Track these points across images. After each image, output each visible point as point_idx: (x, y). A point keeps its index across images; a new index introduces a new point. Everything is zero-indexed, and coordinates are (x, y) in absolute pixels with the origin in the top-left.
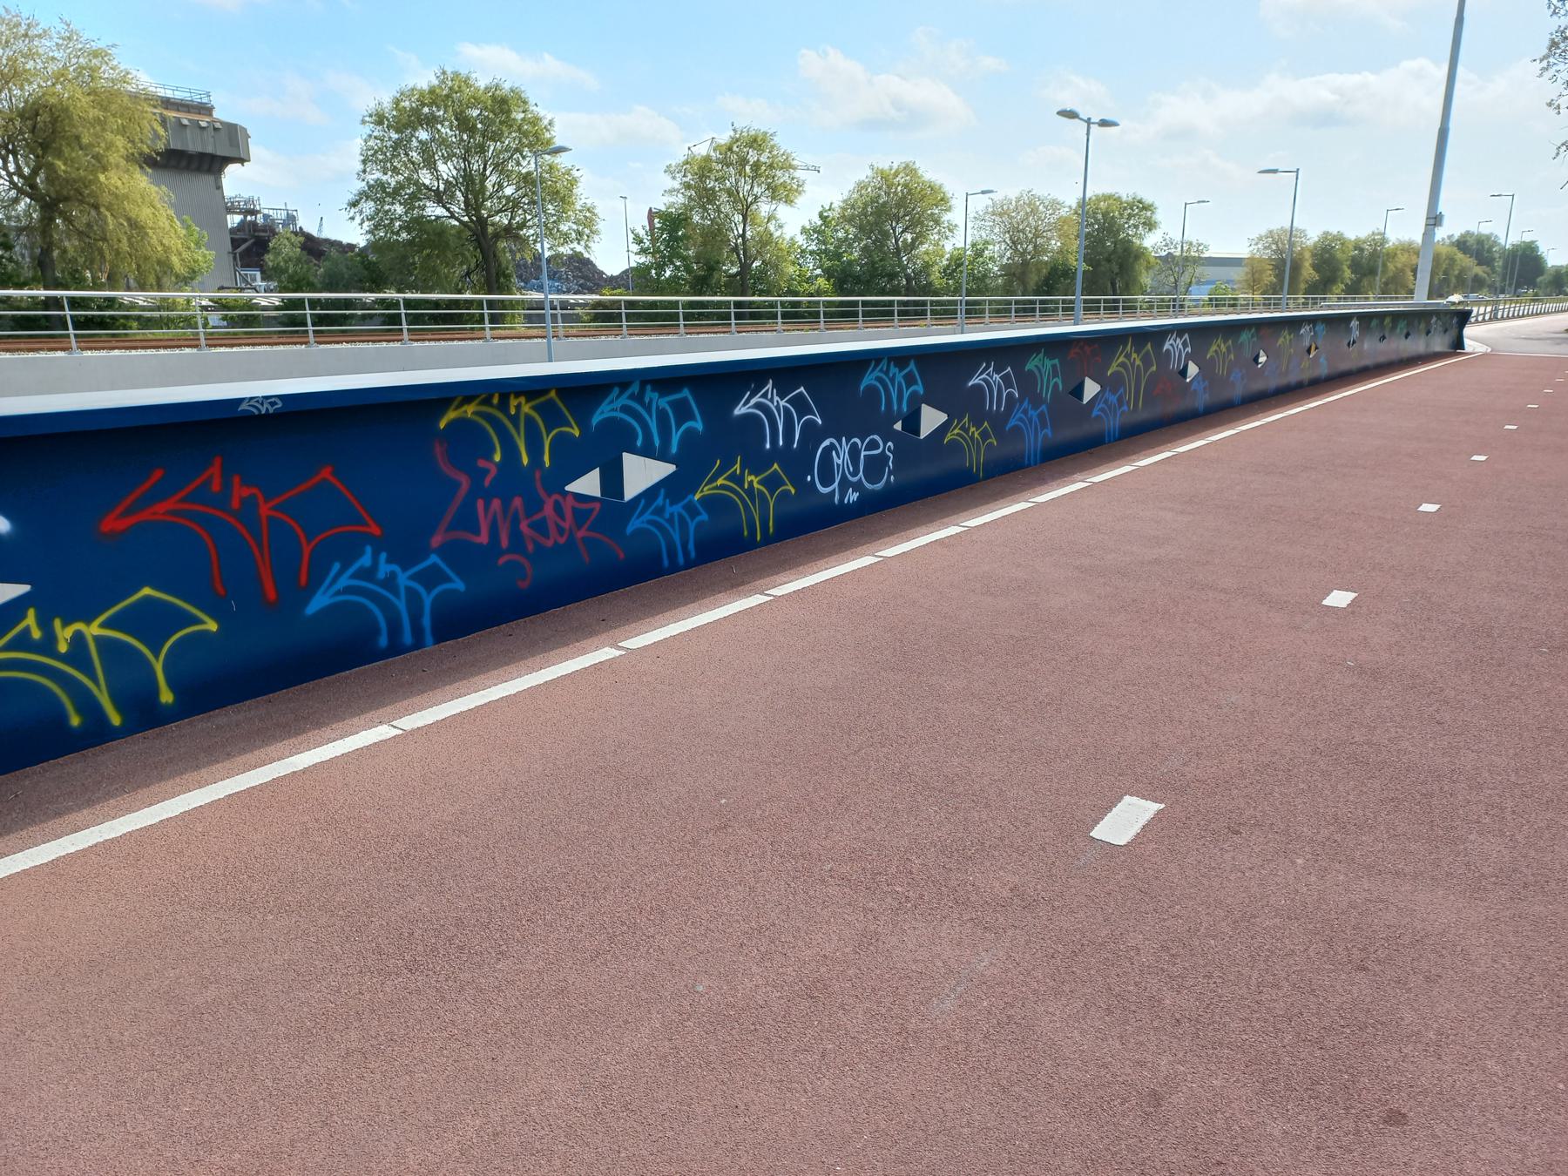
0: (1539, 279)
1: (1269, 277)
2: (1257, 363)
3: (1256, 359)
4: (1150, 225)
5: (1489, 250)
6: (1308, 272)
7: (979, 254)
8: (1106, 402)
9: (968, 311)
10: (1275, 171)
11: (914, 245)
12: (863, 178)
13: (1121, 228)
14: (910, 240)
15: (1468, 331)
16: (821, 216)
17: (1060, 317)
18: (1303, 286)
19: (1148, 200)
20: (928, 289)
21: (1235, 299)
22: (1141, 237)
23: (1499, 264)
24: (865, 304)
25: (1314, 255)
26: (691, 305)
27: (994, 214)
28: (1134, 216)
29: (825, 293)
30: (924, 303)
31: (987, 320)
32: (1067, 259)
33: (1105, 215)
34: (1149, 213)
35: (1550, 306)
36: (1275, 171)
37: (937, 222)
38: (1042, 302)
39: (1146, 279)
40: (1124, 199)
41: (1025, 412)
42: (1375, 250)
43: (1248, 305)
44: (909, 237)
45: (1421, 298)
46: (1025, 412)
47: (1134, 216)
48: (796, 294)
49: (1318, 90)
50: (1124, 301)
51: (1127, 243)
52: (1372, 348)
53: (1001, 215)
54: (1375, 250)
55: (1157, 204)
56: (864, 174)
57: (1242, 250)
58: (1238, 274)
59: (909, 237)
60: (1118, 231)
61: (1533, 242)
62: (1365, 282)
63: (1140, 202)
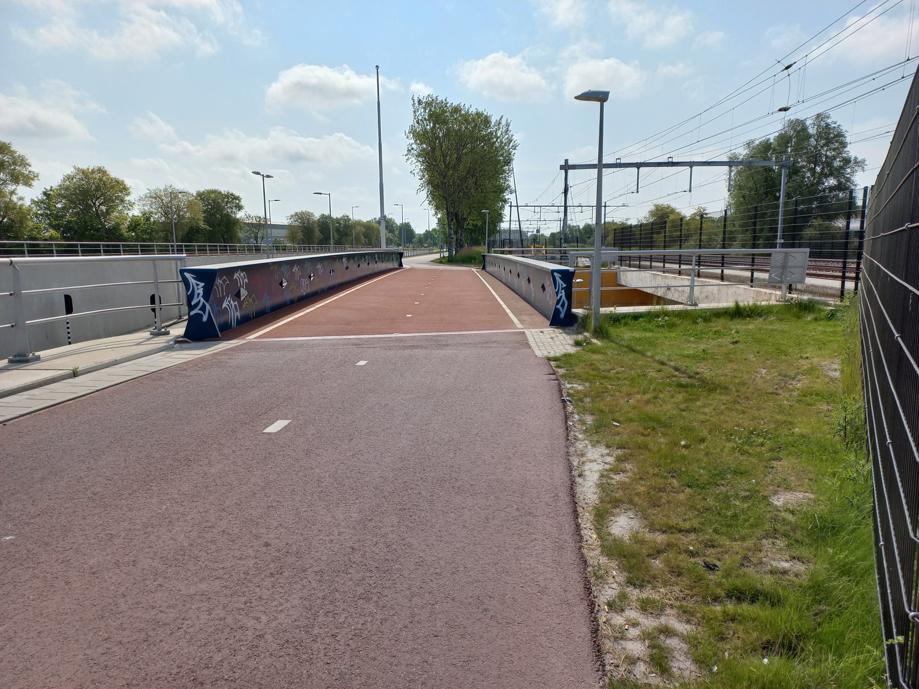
0: (414, 240)
1: (300, 236)
2: (282, 286)
3: (281, 284)
4: (240, 208)
5: (392, 226)
6: (317, 233)
7: (148, 219)
8: (248, 302)
9: (255, 250)
10: (321, 194)
11: (108, 212)
12: (70, 173)
13: (223, 209)
14: (105, 211)
15: (403, 260)
16: (45, 193)
17: (219, 254)
18: (316, 240)
19: (237, 194)
20: (120, 238)
21: (285, 246)
22: (235, 213)
23: (397, 232)
24: (82, 246)
25: (319, 226)
26: (107, 246)
27: (151, 197)
28: (230, 202)
29: (56, 239)
30: (99, 246)
31: (197, 254)
32: (198, 224)
33: (214, 201)
34: (237, 201)
35: (419, 252)
36: (321, 194)
37: (122, 201)
38: (186, 246)
39: (241, 235)
40: (223, 193)
41: (229, 302)
42: (346, 224)
43: (291, 249)
44: (103, 208)
45: (384, 248)
46: (229, 302)
47: (230, 202)
48: (36, 239)
49: (297, 143)
50: (230, 246)
51: (228, 216)
52: (366, 268)
53: (155, 198)
54: (346, 224)
55: (241, 197)
56: (70, 171)
57: (285, 222)
58: (284, 232)
59: (103, 208)
60: (222, 210)
61: (408, 223)
62: (343, 239)
63: (232, 195)
